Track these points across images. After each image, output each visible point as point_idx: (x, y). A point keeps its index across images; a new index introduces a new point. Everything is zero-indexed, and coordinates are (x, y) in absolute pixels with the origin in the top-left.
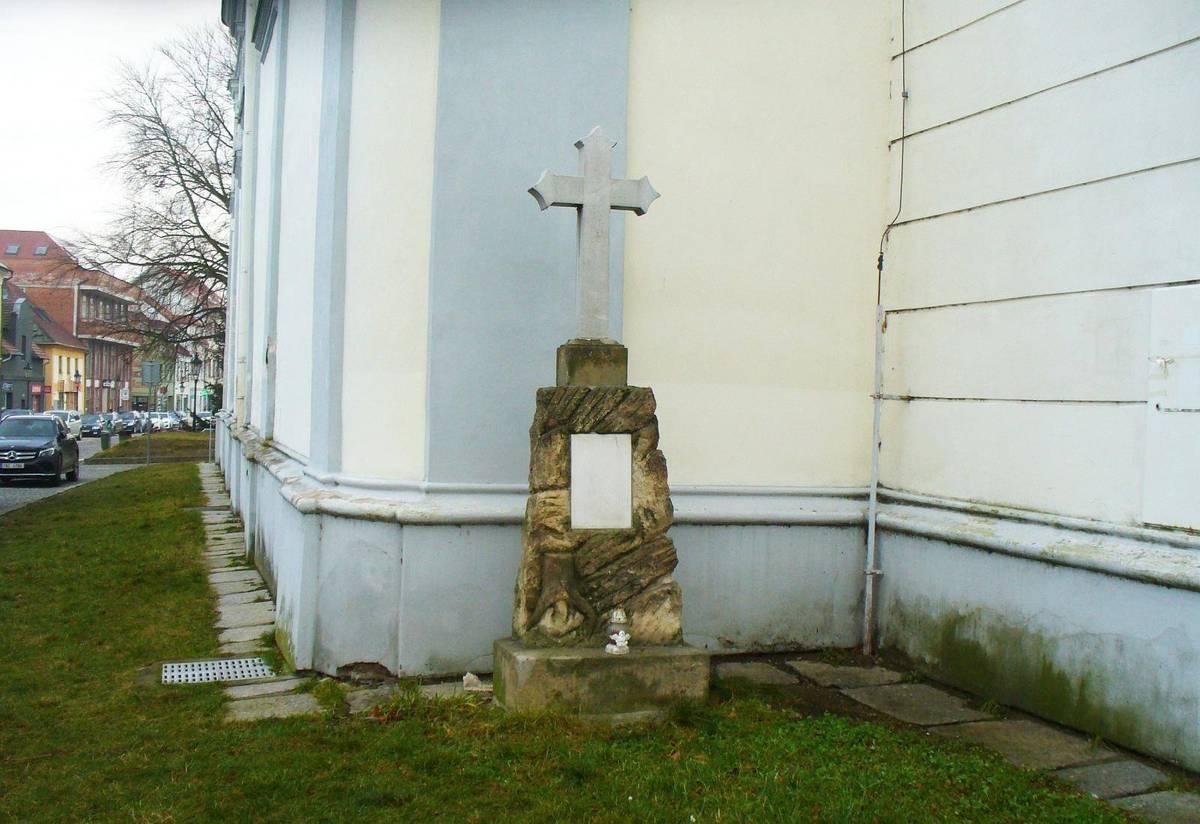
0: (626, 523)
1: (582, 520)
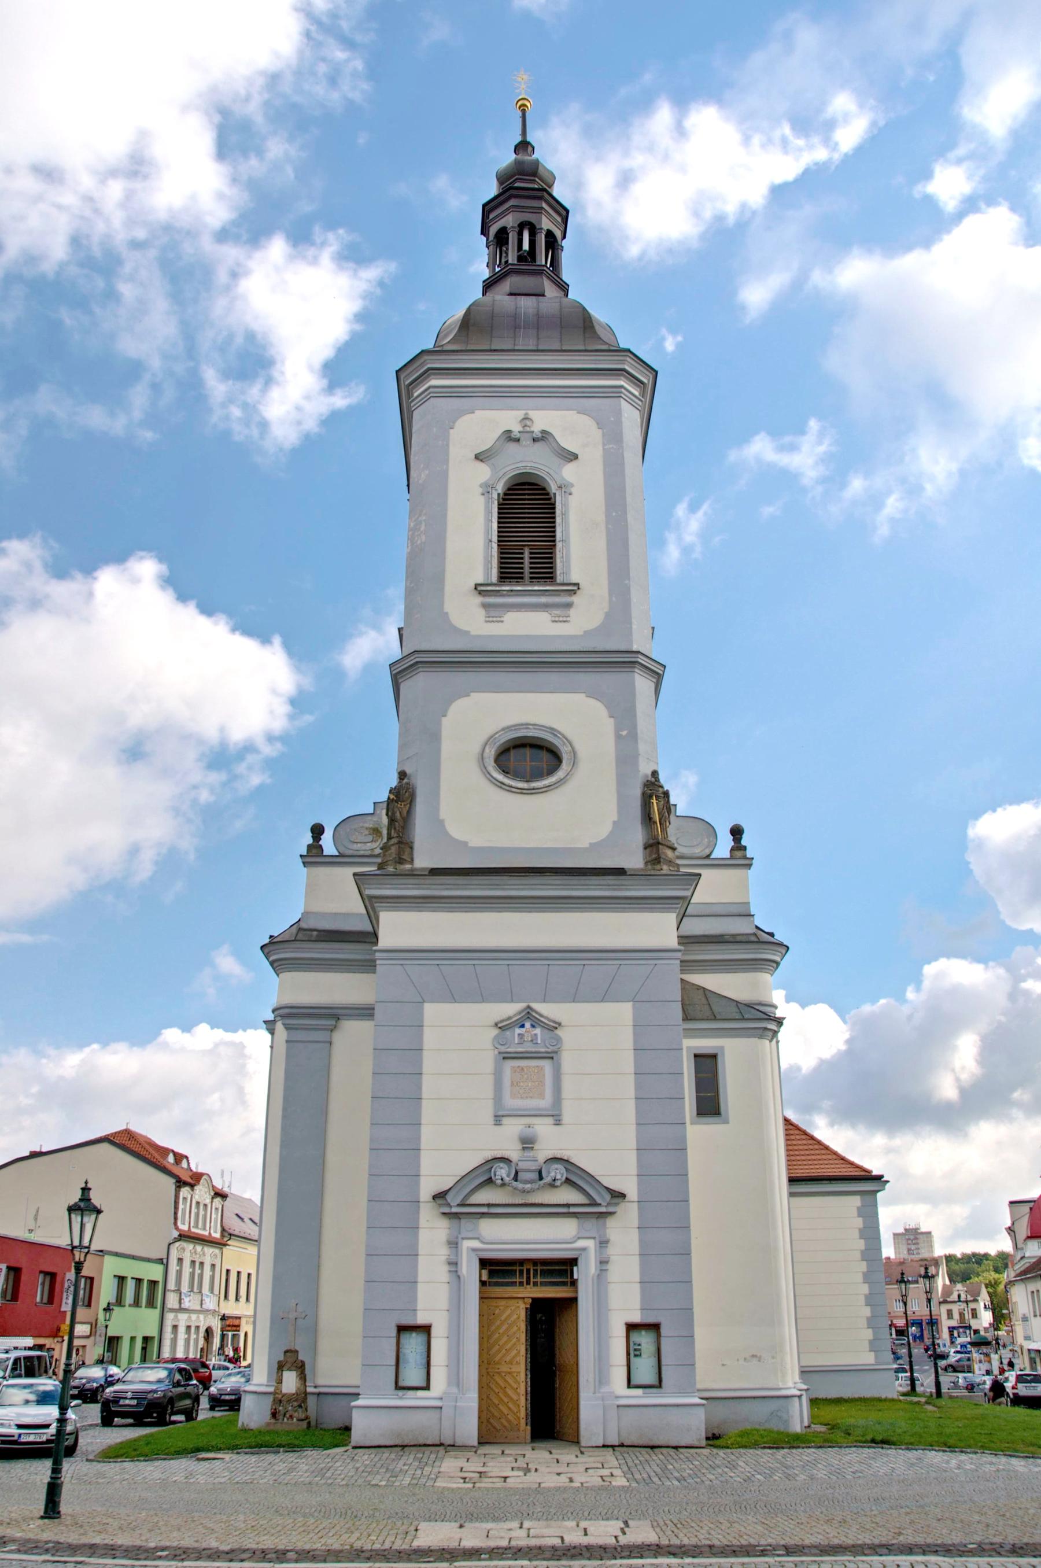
0: (294, 1391)
1: (284, 1391)
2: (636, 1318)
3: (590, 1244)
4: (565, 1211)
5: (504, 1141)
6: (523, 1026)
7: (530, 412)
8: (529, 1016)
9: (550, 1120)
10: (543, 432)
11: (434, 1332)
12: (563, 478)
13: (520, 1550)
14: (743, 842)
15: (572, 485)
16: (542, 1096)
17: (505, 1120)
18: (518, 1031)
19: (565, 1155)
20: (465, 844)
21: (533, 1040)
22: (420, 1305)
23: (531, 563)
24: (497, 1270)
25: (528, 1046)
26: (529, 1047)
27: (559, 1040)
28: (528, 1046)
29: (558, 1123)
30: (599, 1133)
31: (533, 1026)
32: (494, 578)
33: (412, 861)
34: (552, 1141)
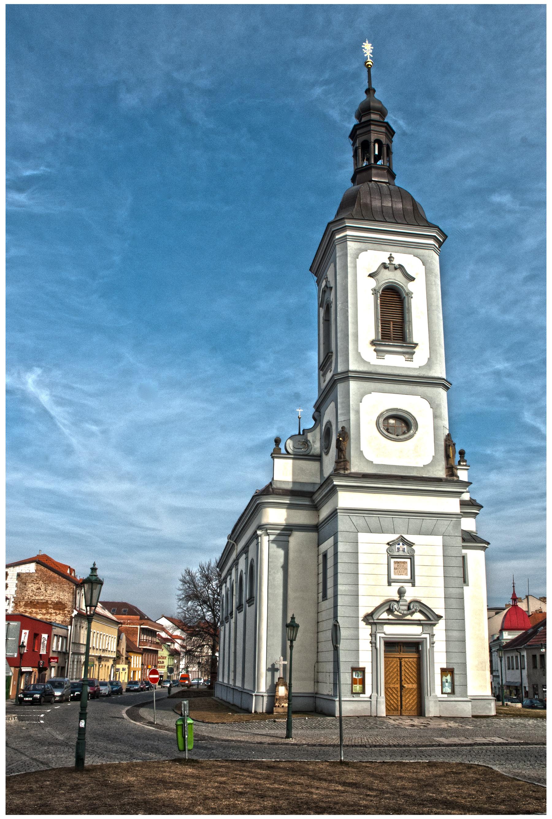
2: (445, 666)
3: (427, 636)
4: (418, 623)
5: (392, 593)
6: (399, 544)
7: (392, 253)
8: (403, 540)
9: (410, 584)
10: (400, 265)
11: (366, 671)
12: (408, 290)
13: (494, 772)
14: (465, 458)
15: (412, 293)
16: (406, 574)
17: (392, 584)
18: (397, 546)
19: (418, 599)
20: (372, 462)
21: (404, 551)
22: (360, 660)
23: (393, 329)
24: (391, 645)
25: (401, 554)
26: (401, 553)
27: (414, 551)
28: (401, 554)
29: (413, 585)
30: (430, 590)
31: (403, 545)
32: (380, 338)
33: (350, 469)
34: (411, 594)
